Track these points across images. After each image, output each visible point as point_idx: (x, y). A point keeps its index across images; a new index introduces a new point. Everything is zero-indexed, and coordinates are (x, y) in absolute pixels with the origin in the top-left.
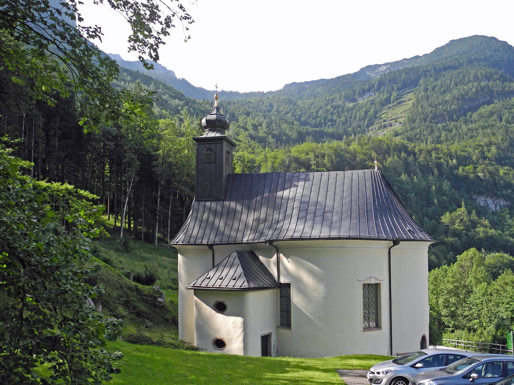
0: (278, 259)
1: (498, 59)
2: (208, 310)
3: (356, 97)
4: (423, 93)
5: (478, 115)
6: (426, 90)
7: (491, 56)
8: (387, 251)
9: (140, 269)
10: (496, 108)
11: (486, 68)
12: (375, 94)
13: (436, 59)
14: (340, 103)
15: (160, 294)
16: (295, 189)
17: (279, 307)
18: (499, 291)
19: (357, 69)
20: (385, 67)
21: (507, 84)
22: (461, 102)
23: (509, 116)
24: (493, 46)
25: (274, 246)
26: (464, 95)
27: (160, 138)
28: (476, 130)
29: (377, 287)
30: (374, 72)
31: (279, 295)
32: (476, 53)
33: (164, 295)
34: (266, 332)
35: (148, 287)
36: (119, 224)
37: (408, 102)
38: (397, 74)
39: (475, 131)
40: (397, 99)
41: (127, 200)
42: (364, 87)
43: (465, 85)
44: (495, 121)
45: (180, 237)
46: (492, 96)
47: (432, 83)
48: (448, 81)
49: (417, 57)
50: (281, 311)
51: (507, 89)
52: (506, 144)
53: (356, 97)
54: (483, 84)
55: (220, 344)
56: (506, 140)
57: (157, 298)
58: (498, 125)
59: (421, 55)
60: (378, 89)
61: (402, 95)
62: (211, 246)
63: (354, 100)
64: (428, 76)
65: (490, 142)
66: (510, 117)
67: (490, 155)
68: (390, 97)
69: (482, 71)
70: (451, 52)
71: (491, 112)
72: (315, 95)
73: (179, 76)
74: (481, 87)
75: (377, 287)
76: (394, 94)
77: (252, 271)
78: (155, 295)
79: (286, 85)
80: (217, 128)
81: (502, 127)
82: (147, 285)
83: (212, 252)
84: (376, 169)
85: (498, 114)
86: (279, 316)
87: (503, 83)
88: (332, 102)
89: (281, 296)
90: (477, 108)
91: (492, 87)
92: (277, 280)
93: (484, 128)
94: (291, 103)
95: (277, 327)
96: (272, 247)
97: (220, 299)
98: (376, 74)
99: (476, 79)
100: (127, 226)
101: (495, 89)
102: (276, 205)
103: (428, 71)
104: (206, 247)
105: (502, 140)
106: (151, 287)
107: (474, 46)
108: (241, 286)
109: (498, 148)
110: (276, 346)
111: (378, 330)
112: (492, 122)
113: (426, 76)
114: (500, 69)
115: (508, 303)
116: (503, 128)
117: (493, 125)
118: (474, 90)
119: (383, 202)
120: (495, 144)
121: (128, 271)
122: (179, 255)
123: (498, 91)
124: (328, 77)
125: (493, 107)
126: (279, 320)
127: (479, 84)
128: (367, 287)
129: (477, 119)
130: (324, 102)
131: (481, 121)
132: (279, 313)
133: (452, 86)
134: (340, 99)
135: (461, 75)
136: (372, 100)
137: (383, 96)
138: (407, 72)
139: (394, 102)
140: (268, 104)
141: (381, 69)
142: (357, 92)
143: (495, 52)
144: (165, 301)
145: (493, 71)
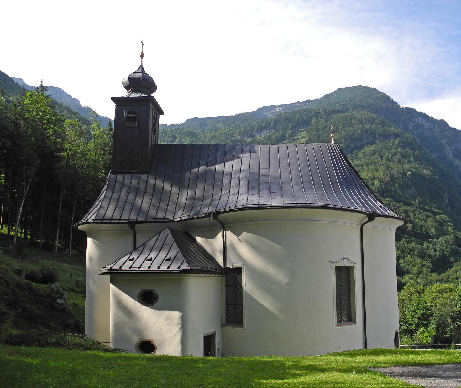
0: (224, 237)
1: (378, 107)
2: (131, 302)
3: (254, 133)
4: (314, 132)
5: (363, 153)
6: (317, 130)
7: (373, 104)
8: (359, 229)
9: (35, 268)
10: (378, 148)
11: (369, 113)
12: (271, 131)
13: (326, 104)
14: (239, 137)
15: (60, 294)
16: (239, 160)
17: (224, 299)
18: (404, 300)
19: (255, 109)
20: (280, 109)
21: (387, 128)
22: (348, 141)
23: (389, 155)
24: (375, 96)
25: (220, 221)
26: (350, 136)
27: (64, 139)
28: (362, 166)
29: (349, 270)
30: (270, 112)
31: (224, 284)
32: (360, 101)
33: (65, 296)
34: (209, 331)
35: (44, 286)
36: (12, 234)
37: (301, 140)
38: (292, 114)
39: (360, 167)
40: (292, 137)
41: (23, 201)
42: (261, 124)
43: (352, 126)
44: (377, 159)
45: (91, 217)
46: (374, 138)
47: (323, 123)
48: (337, 123)
49: (309, 101)
50: (227, 304)
51: (386, 132)
52: (387, 179)
53: (254, 133)
54: (367, 126)
55: (147, 346)
56: (387, 175)
57: (57, 298)
58: (380, 162)
59: (313, 100)
60: (275, 127)
61: (296, 133)
62: (132, 225)
63: (252, 136)
64: (319, 117)
65: (374, 176)
66: (390, 156)
67: (374, 188)
68: (285, 135)
69: (366, 114)
70: (338, 98)
71: (373, 151)
72: (216, 129)
73: (84, 103)
74: (365, 129)
75: (349, 270)
76: (289, 132)
77: (190, 251)
78: (53, 295)
79: (189, 120)
80: (142, 89)
81: (383, 165)
82: (43, 283)
83: (134, 231)
84: (333, 142)
85: (379, 153)
86: (224, 312)
87: (383, 126)
88: (232, 137)
89: (227, 286)
90: (361, 147)
91: (374, 130)
92: (222, 264)
93: (368, 164)
94: (193, 136)
95: (223, 325)
96: (216, 221)
97: (148, 287)
98: (272, 114)
99: (361, 122)
100: (23, 236)
101: (377, 132)
102: (214, 180)
103: (319, 113)
104: (126, 225)
105: (384, 175)
106: (48, 285)
107: (359, 94)
108: (179, 268)
109: (380, 182)
110: (220, 350)
111: (350, 324)
112: (374, 159)
113: (317, 117)
114: (380, 115)
115: (415, 311)
116: (385, 165)
117: (376, 163)
118: (359, 131)
119: (346, 176)
120: (378, 179)
121: (19, 269)
122: (89, 241)
123: (379, 134)
124: (228, 113)
125: (376, 147)
126: (224, 315)
127: (363, 127)
128: (339, 269)
129: (362, 157)
130: (224, 136)
131: (365, 159)
132: (224, 308)
133: (340, 127)
134: (239, 134)
135: (348, 119)
136: (268, 137)
137: (279, 133)
138: (301, 113)
139: (288, 139)
140: (171, 135)
141: (277, 110)
142: (255, 129)
143: (376, 101)
144: (66, 303)
145: (375, 116)
